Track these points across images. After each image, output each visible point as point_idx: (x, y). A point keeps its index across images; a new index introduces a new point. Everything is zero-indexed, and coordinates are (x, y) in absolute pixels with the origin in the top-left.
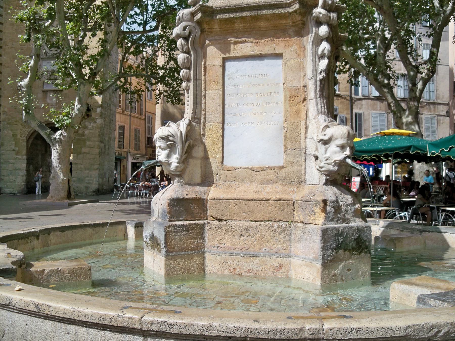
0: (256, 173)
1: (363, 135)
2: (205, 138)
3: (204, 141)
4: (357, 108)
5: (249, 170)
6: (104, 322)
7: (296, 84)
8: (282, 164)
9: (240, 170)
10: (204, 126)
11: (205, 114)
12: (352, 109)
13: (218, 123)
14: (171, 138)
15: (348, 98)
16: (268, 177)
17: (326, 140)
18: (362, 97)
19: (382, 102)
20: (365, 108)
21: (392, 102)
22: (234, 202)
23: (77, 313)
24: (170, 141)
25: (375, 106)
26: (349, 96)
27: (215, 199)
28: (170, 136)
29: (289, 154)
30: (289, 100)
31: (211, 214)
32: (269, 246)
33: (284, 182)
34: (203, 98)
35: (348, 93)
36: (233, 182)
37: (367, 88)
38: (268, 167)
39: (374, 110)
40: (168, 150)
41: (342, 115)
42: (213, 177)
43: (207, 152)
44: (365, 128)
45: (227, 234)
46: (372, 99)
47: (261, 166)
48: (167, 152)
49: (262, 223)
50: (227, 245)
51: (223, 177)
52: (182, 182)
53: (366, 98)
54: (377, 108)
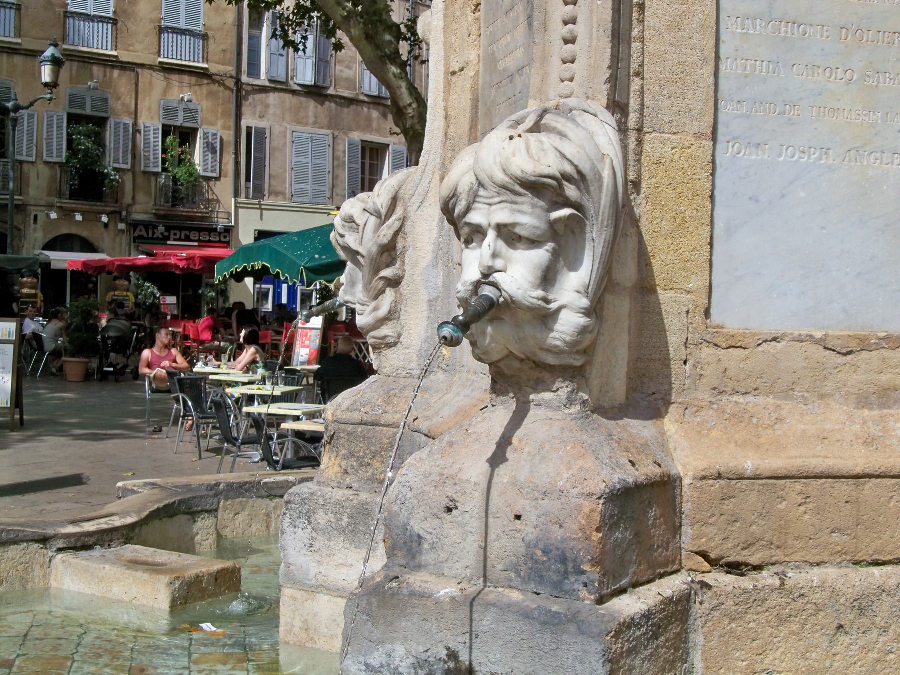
0: (842, 360)
1: (266, 192)
2: (640, 199)
3: (637, 211)
4: (254, 114)
5: (812, 349)
9: (779, 346)
10: (640, 143)
11: (642, 92)
12: (239, 117)
13: (699, 136)
14: (571, 191)
15: (231, 83)
16: (883, 378)
18: (267, 84)
19: (322, 104)
20: (275, 114)
21: (410, 105)
22: (798, 486)
25: (302, 114)
26: (232, 77)
27: (720, 476)
28: (567, 178)
31: (702, 544)
34: (635, 15)
35: (231, 69)
36: (750, 398)
37: (283, 60)
38: (883, 339)
39: (299, 123)
40: (550, 246)
41: (211, 130)
42: (669, 376)
43: (649, 265)
44: (273, 173)
45: (784, 631)
46: (294, 92)
48: (541, 255)
51: (711, 375)
52: (584, 403)
53: (279, 86)
54: (307, 117)
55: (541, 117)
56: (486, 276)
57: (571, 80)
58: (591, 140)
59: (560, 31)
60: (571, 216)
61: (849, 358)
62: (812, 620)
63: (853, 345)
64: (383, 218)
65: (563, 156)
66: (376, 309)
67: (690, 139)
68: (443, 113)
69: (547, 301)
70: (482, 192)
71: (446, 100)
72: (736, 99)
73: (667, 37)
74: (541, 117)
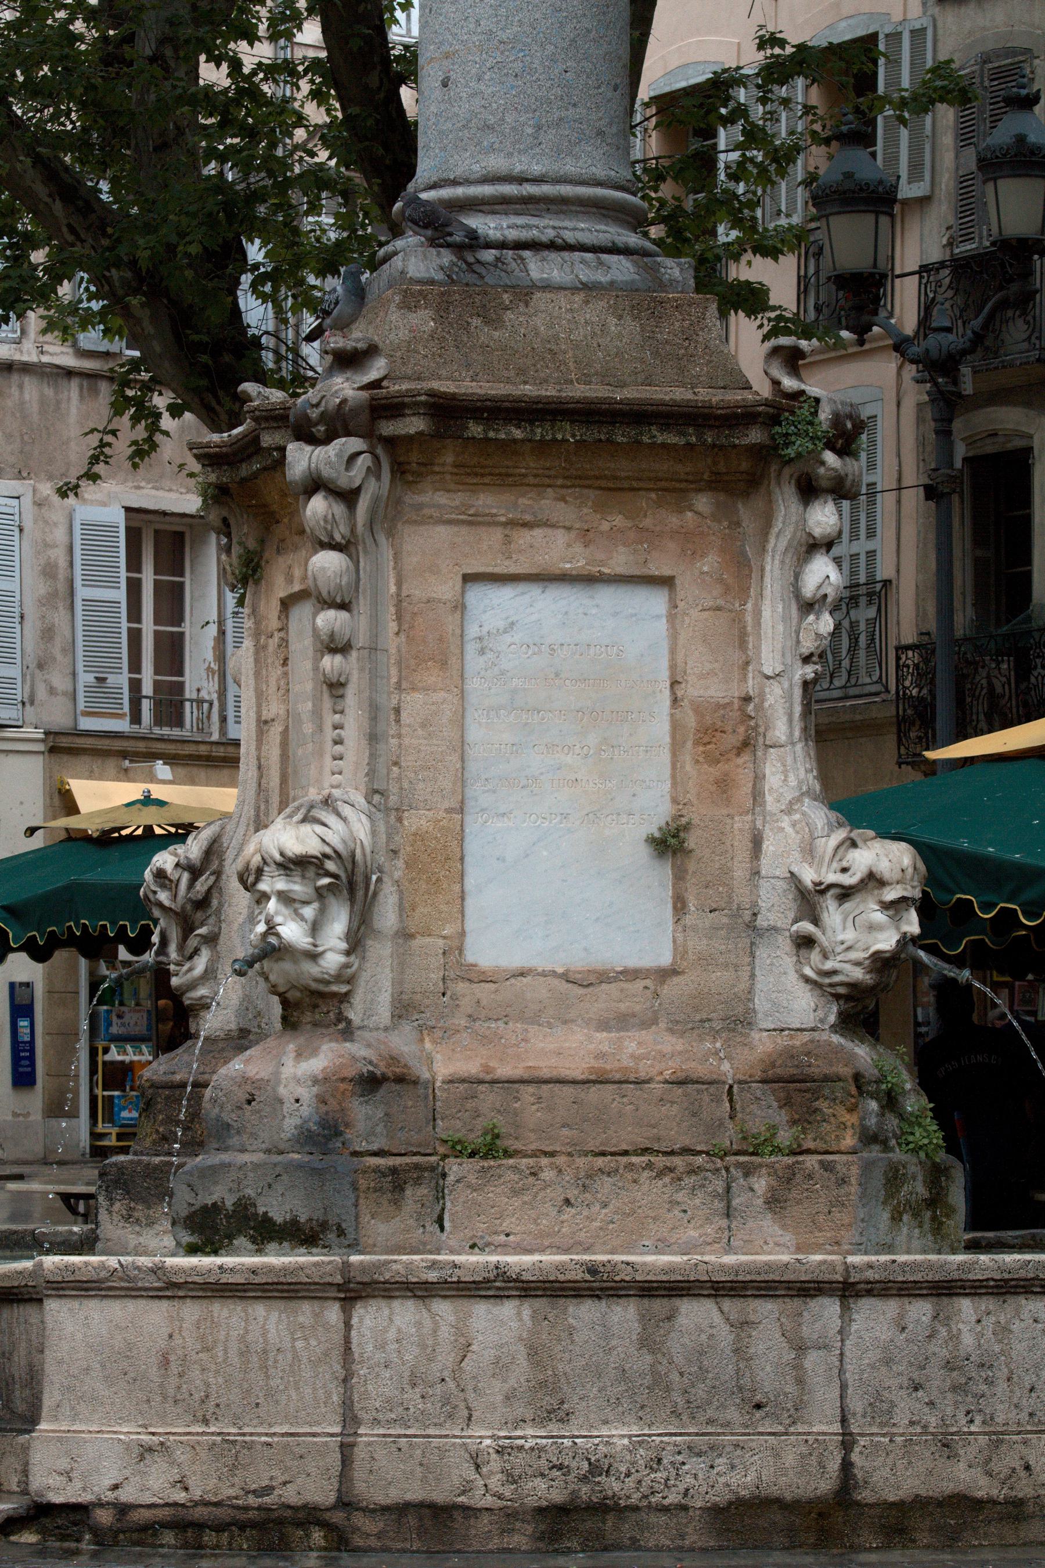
0: (581, 991)
5: (556, 982)
6: (771, 1277)
7: (710, 688)
8: (665, 958)
17: (851, 887)
22: (531, 1089)
23: (702, 1267)
24: (328, 874)
28: (326, 856)
29: (694, 928)
30: (697, 743)
32: (659, 1235)
33: (677, 1022)
38: (621, 973)
47: (599, 967)
49: (624, 1160)
50: (518, 1238)
51: (466, 1005)
55: (309, 811)
56: (270, 928)
57: (340, 773)
58: (351, 828)
59: (330, 734)
60: (330, 884)
61: (591, 988)
62: (542, 1194)
63: (592, 979)
64: (195, 872)
65: (323, 841)
66: (190, 970)
67: (442, 814)
68: (255, 762)
69: (315, 946)
70: (266, 869)
71: (259, 748)
72: (483, 777)
73: (420, 732)
74: (309, 811)
